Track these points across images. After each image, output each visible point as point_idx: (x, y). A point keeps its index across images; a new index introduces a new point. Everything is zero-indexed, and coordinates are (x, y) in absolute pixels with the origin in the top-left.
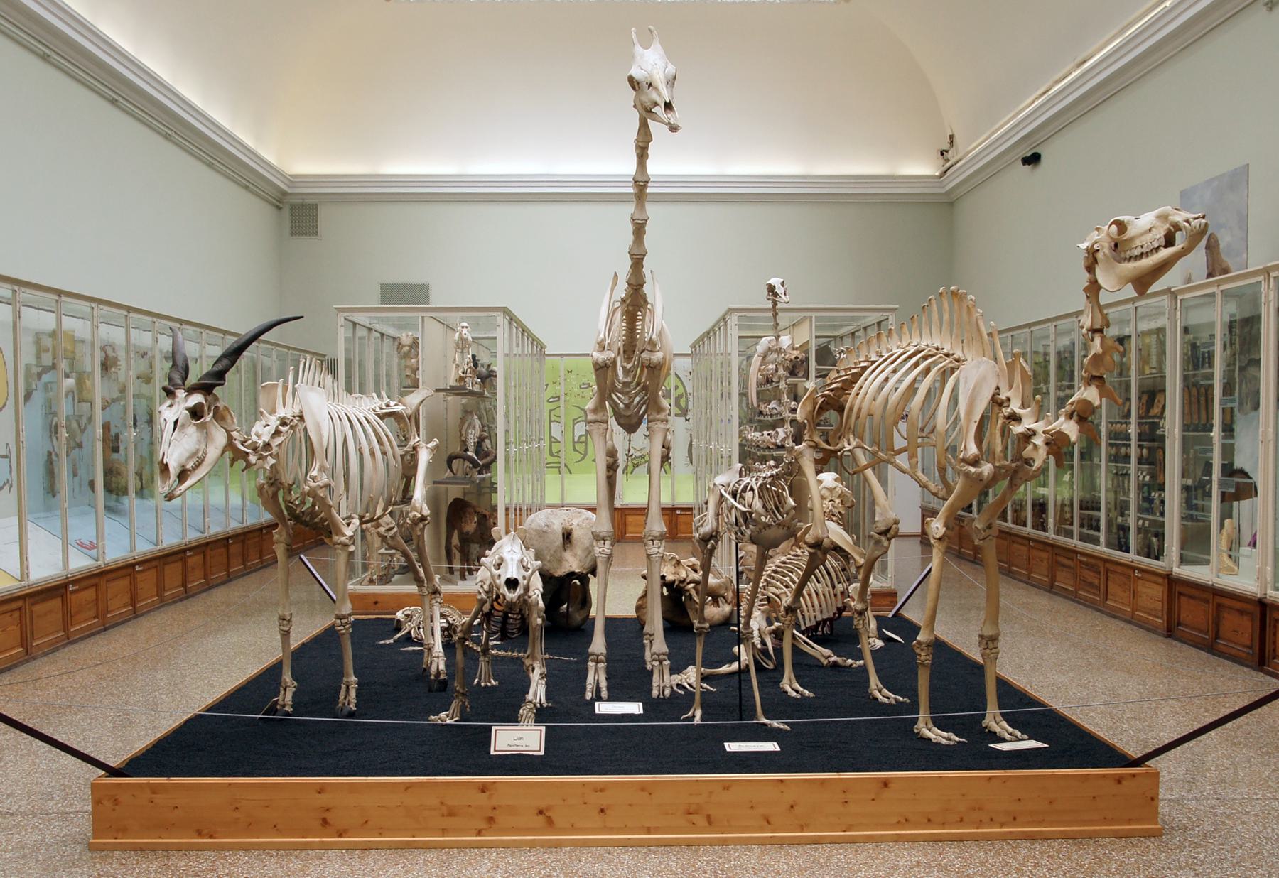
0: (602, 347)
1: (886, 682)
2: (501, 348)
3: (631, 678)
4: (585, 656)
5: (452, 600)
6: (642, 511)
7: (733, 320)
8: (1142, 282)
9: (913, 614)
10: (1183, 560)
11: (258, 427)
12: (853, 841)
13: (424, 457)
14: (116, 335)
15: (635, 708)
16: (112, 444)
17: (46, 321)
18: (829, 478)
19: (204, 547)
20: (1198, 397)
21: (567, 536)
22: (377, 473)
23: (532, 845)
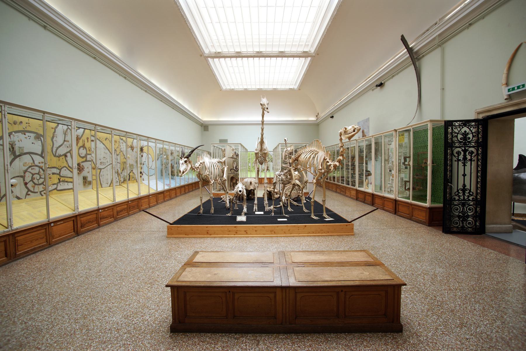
0: (256, 150)
1: (306, 208)
2: (240, 150)
3: (261, 207)
4: (254, 204)
5: (231, 194)
6: (264, 178)
7: (280, 145)
8: (350, 138)
9: (311, 196)
10: (359, 187)
11: (196, 164)
12: (300, 236)
13: (226, 169)
14: (173, 148)
15: (262, 213)
16: (172, 167)
17: (161, 146)
18: (296, 173)
19: (188, 185)
20: (361, 158)
21: (251, 183)
22: (217, 172)
23: (244, 237)
